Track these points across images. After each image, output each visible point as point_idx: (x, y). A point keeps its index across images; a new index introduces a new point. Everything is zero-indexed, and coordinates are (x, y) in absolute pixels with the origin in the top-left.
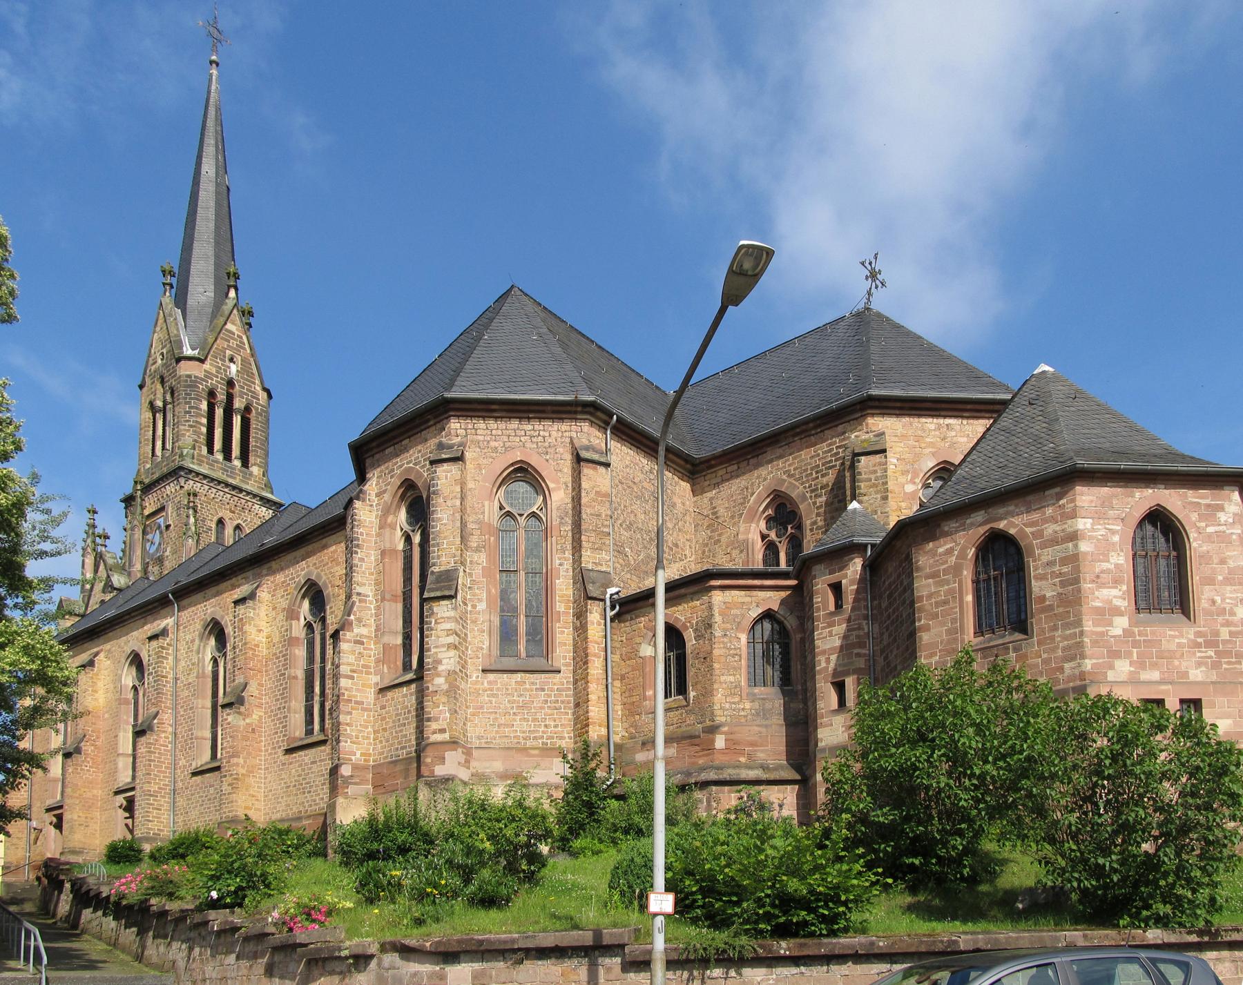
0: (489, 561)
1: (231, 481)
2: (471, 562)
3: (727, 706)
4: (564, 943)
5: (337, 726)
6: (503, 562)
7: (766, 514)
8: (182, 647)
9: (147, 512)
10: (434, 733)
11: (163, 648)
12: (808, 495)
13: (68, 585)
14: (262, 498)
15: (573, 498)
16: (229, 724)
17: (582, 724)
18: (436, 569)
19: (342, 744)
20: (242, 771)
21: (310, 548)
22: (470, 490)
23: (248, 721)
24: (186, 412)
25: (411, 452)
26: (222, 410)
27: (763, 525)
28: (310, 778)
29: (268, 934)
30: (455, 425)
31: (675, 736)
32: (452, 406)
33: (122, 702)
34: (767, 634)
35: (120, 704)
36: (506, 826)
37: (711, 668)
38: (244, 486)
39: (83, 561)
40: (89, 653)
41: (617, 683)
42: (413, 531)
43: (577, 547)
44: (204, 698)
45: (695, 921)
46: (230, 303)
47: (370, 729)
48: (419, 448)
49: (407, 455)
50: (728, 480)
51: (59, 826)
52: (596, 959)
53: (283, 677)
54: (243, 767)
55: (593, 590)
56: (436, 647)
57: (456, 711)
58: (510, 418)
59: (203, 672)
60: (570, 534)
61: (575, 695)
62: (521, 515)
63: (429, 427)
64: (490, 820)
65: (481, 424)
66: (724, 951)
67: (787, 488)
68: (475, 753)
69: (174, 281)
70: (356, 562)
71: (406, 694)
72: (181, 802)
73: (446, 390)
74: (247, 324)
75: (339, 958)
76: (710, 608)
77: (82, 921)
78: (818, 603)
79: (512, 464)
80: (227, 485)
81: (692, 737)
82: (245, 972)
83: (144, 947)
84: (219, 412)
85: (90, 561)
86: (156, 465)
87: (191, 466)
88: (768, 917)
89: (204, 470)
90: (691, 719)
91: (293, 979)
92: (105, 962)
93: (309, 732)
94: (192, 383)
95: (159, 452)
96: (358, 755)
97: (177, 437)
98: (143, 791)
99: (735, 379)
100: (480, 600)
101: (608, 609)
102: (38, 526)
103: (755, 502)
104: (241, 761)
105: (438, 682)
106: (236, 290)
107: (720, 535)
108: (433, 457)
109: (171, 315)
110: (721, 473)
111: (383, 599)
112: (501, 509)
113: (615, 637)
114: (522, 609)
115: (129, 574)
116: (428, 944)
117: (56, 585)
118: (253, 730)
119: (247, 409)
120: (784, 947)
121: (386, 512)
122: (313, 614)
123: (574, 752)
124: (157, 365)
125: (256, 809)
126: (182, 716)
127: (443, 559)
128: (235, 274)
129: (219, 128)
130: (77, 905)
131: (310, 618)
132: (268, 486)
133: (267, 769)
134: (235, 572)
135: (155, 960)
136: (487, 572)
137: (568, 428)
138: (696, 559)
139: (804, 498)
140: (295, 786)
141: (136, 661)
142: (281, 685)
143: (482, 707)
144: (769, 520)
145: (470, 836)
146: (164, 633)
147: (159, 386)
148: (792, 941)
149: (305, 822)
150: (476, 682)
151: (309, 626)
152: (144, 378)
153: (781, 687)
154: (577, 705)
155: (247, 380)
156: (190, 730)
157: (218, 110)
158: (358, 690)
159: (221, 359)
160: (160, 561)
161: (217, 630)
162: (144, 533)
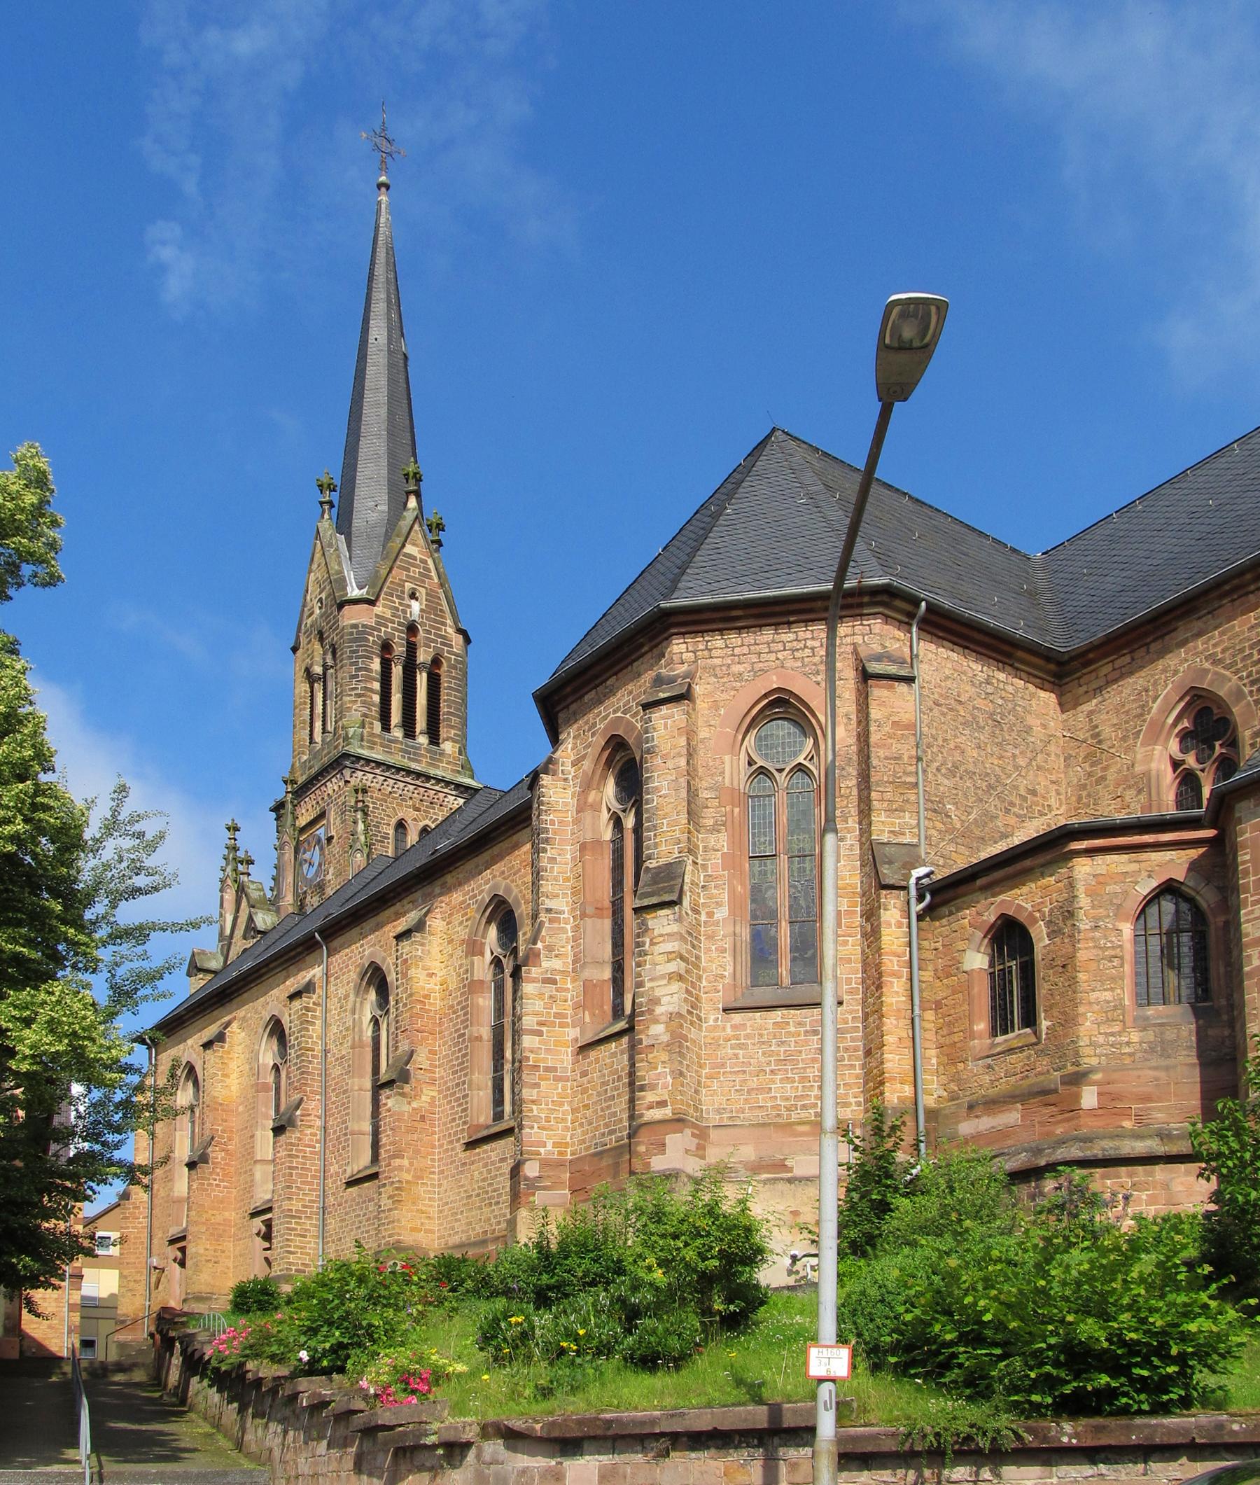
0: (732, 843)
1: (414, 766)
2: (706, 849)
3: (1101, 1039)
4: (725, 1426)
5: (517, 1103)
6: (754, 844)
7: (1179, 727)
8: (333, 1004)
9: (302, 822)
10: (650, 1107)
11: (307, 1009)
12: (1246, 690)
13: (168, 932)
14: (458, 786)
15: (859, 735)
16: (389, 1110)
17: (875, 1081)
18: (652, 864)
19: (526, 1131)
20: (407, 1177)
21: (496, 850)
22: (703, 741)
23: (415, 1105)
24: (352, 677)
25: (619, 695)
26: (400, 668)
27: (1174, 746)
28: (499, 1183)
29: (356, 1412)
30: (679, 647)
31: (1017, 1092)
32: (673, 619)
33: (261, 1088)
34: (1167, 920)
35: (257, 1091)
36: (686, 1244)
37: (1073, 982)
38: (433, 772)
39: (222, 897)
40: (219, 1023)
41: (930, 1015)
42: (624, 811)
43: (865, 811)
44: (361, 1076)
45: (950, 1389)
46: (409, 516)
47: (566, 1107)
48: (630, 687)
49: (613, 699)
50: (1115, 681)
51: (182, 1264)
52: (776, 1449)
53: (463, 1039)
54: (408, 1171)
55: (889, 874)
56: (651, 980)
57: (681, 1074)
58: (761, 626)
59: (361, 1040)
60: (855, 792)
61: (866, 1036)
62: (780, 771)
63: (642, 656)
64: (663, 1236)
65: (717, 641)
66: (969, 1438)
67: (1212, 682)
68: (713, 1134)
69: (335, 497)
70: (544, 863)
71: (615, 1053)
72: (332, 1224)
73: (666, 597)
74: (433, 542)
75: (426, 1447)
76: (1071, 885)
77: (190, 1394)
78: (1245, 862)
79: (765, 696)
80: (409, 772)
81: (1045, 1092)
82: (334, 1466)
83: (243, 1429)
84: (397, 671)
85: (230, 896)
86: (314, 755)
87: (360, 751)
88: (1048, 1383)
89: (377, 755)
90: (1043, 1064)
91: (380, 1477)
92: (195, 1450)
93: (498, 1116)
94: (360, 634)
95: (318, 737)
96: (549, 1147)
97: (341, 713)
98: (283, 1212)
99: (1135, 521)
100: (719, 904)
101: (913, 901)
102: (125, 855)
103: (1160, 711)
104: (406, 1162)
105: (656, 1032)
106: (418, 494)
107: (1105, 769)
108: (644, 699)
109: (330, 545)
110: (1105, 670)
111: (583, 915)
112: (750, 764)
113: (925, 943)
114: (784, 912)
115: (278, 911)
116: (538, 1427)
117: (152, 934)
118: (423, 1117)
119: (436, 662)
120: (1067, 1432)
121: (587, 785)
122: (503, 945)
123: (863, 1125)
124: (314, 616)
125: (427, 1231)
126: (334, 1103)
127: (662, 850)
128: (415, 474)
129: (392, 276)
130: (185, 1372)
131: (498, 951)
132: (467, 768)
133: (442, 1172)
134: (399, 894)
135: (253, 1448)
136: (730, 861)
137: (849, 631)
138: (1069, 810)
139: (1239, 695)
140: (478, 1195)
141: (277, 1029)
142: (460, 1050)
143: (723, 1065)
144: (1184, 737)
145: (635, 1261)
146: (309, 988)
147: (317, 646)
148: (1084, 1421)
149: (492, 1247)
150: (715, 1028)
151: (497, 962)
152: (298, 638)
153: (1192, 1005)
154: (868, 1053)
155: (435, 621)
156: (344, 1122)
157: (390, 251)
158: (548, 1051)
159: (398, 597)
160: (321, 887)
161: (376, 979)
162: (296, 852)
